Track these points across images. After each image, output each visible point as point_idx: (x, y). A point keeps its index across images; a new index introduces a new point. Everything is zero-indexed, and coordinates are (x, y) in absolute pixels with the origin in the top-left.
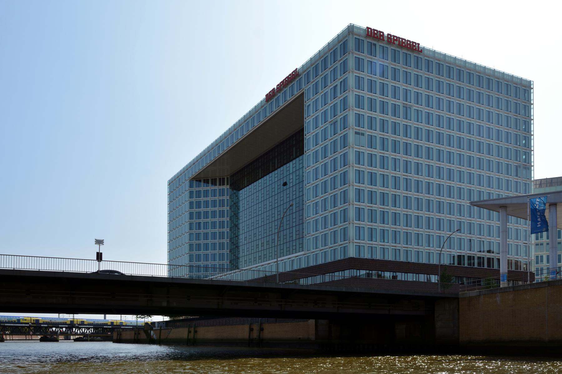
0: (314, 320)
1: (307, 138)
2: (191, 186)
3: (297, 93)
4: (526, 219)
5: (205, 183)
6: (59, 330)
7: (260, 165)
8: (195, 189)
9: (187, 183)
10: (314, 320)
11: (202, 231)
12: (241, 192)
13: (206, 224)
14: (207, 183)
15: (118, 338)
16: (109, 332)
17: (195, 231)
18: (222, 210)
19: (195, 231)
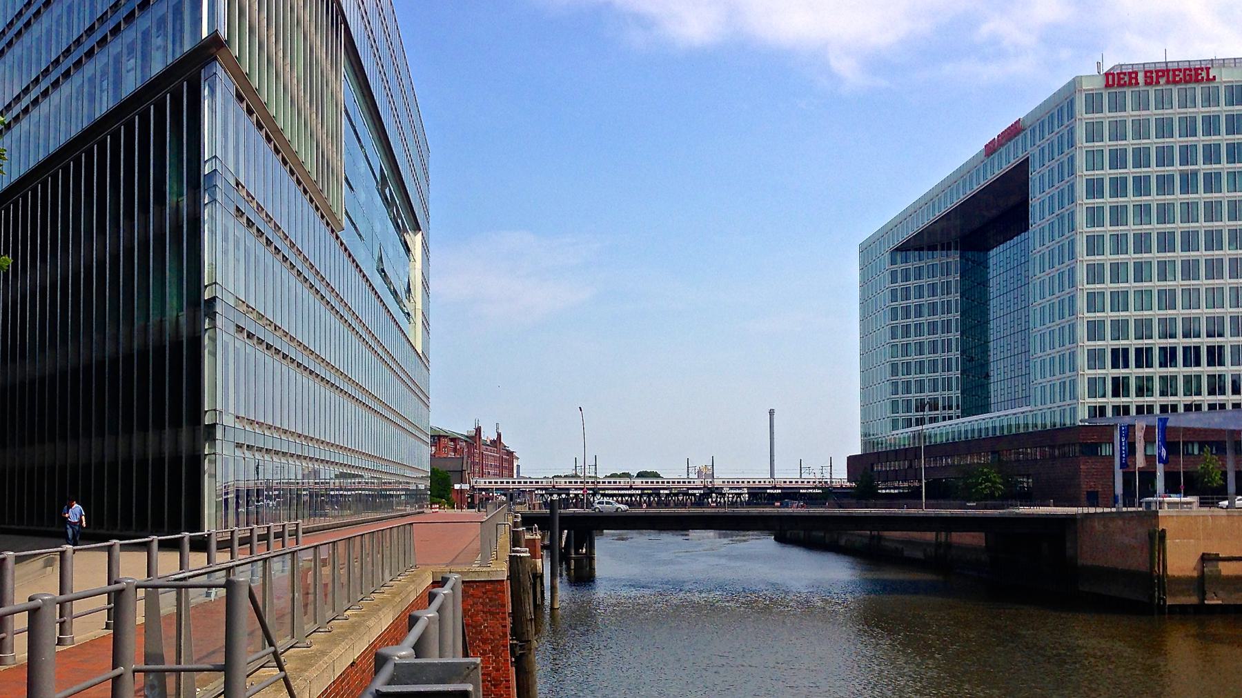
0: (983, 534)
1: (1033, 178)
2: (893, 262)
3: (1021, 156)
4: (1199, 539)
5: (944, 250)
6: (689, 498)
7: (566, 531)
8: (899, 267)
9: (887, 256)
10: (983, 534)
11: (912, 339)
12: (992, 253)
13: (919, 326)
14: (947, 250)
15: (1023, 224)
16: (777, 501)
17: (900, 340)
18: (947, 301)
19: (900, 340)
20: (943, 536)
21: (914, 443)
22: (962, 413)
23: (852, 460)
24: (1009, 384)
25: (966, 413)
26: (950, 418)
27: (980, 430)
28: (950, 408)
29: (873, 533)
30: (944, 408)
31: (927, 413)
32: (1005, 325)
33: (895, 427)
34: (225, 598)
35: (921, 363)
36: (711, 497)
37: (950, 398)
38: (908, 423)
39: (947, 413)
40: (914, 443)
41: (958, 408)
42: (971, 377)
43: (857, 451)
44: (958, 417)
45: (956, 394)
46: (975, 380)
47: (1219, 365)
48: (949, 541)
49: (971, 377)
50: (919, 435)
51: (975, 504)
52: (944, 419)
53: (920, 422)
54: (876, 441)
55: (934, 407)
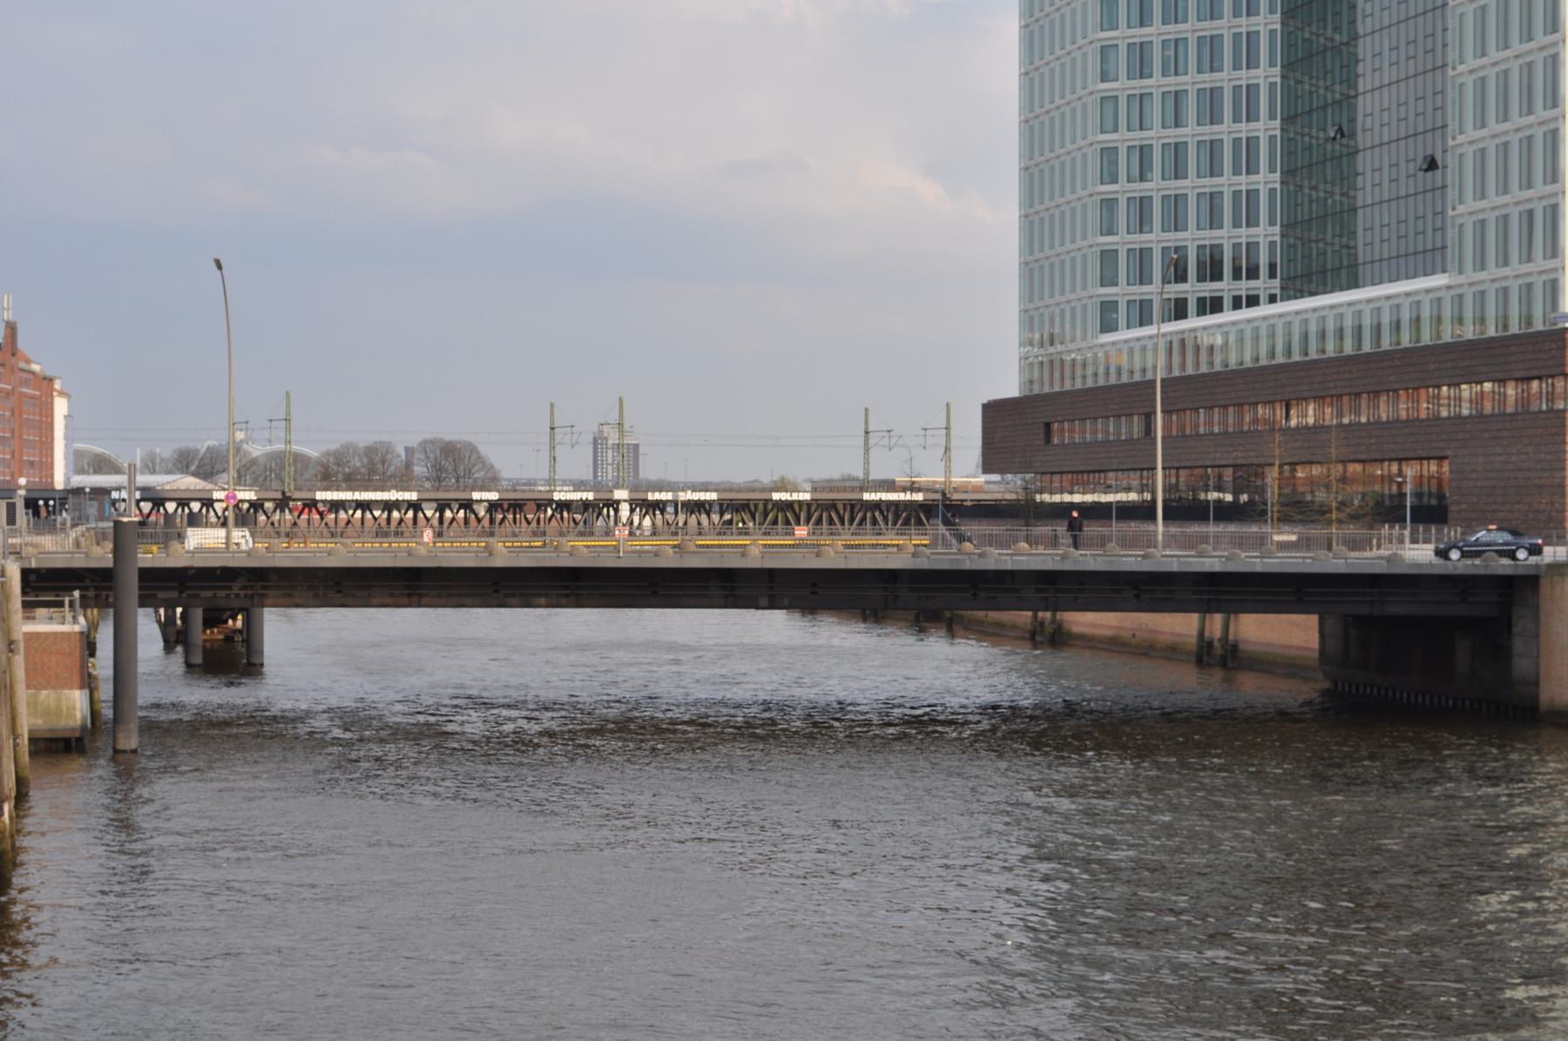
0: (1314, 619)
10: (1314, 619)
11: (1156, 83)
20: (1216, 622)
21: (1183, 366)
22: (1283, 288)
23: (995, 412)
24: (1420, 208)
25: (1293, 288)
26: (1253, 301)
27: (1377, 329)
28: (1253, 273)
29: (1040, 614)
30: (1237, 275)
31: (1192, 289)
32: (1412, 46)
33: (1108, 326)
34: (112, 682)
35: (1178, 149)
36: (546, 511)
37: (1252, 247)
38: (1143, 314)
39: (1244, 287)
40: (1183, 366)
41: (1272, 275)
42: (1306, 191)
43: (1011, 389)
44: (1272, 299)
45: (1266, 234)
46: (1318, 198)
47: (1205, 298)
48: (1231, 637)
49: (1306, 191)
50: (1182, 343)
51: (1293, 538)
52: (1237, 304)
53: (1179, 310)
54: (1150, 344)
55: (1211, 268)
